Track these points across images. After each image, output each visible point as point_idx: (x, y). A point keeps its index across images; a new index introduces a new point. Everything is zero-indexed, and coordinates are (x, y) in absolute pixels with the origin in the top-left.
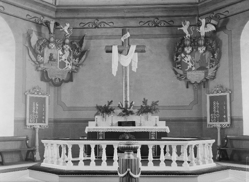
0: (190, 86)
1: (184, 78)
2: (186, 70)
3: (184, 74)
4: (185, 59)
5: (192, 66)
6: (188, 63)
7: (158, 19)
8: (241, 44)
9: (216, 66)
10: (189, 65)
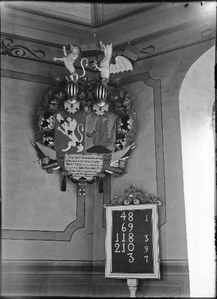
0: (70, 186)
1: (59, 167)
2: (64, 150)
3: (58, 158)
4: (63, 125)
5: (77, 142)
6: (70, 136)
7: (12, 42)
8: (180, 106)
9: (129, 148)
10: (71, 140)
